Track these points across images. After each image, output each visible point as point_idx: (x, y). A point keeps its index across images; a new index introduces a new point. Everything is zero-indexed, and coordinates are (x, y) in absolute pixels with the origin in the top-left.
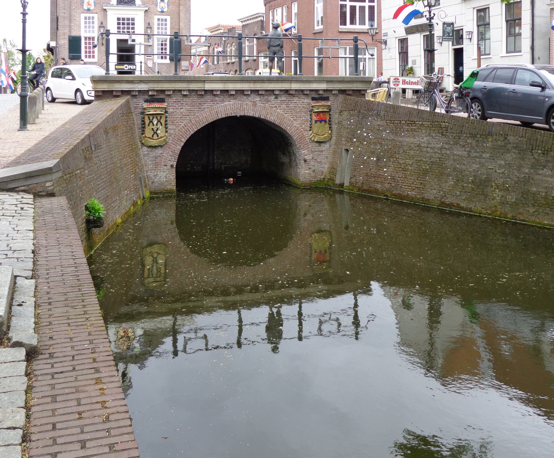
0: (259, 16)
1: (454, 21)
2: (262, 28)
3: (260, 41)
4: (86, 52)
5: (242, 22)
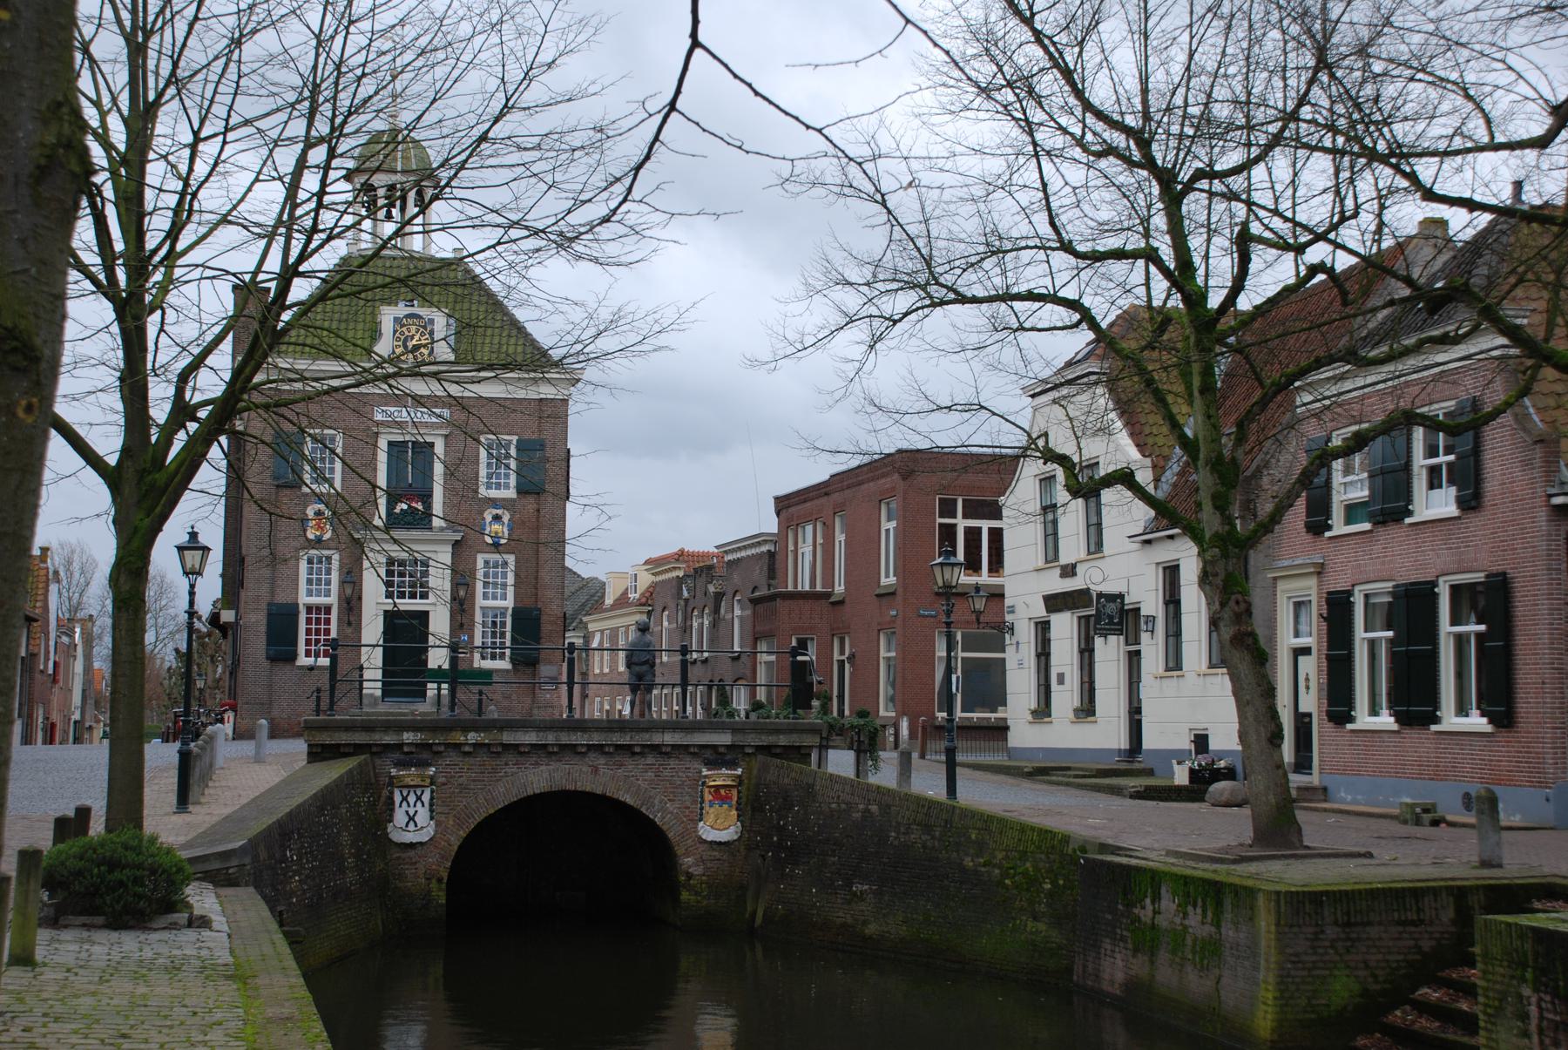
0: (766, 542)
1: (1123, 589)
2: (772, 573)
3: (760, 608)
4: (308, 642)
5: (1033, 396)
